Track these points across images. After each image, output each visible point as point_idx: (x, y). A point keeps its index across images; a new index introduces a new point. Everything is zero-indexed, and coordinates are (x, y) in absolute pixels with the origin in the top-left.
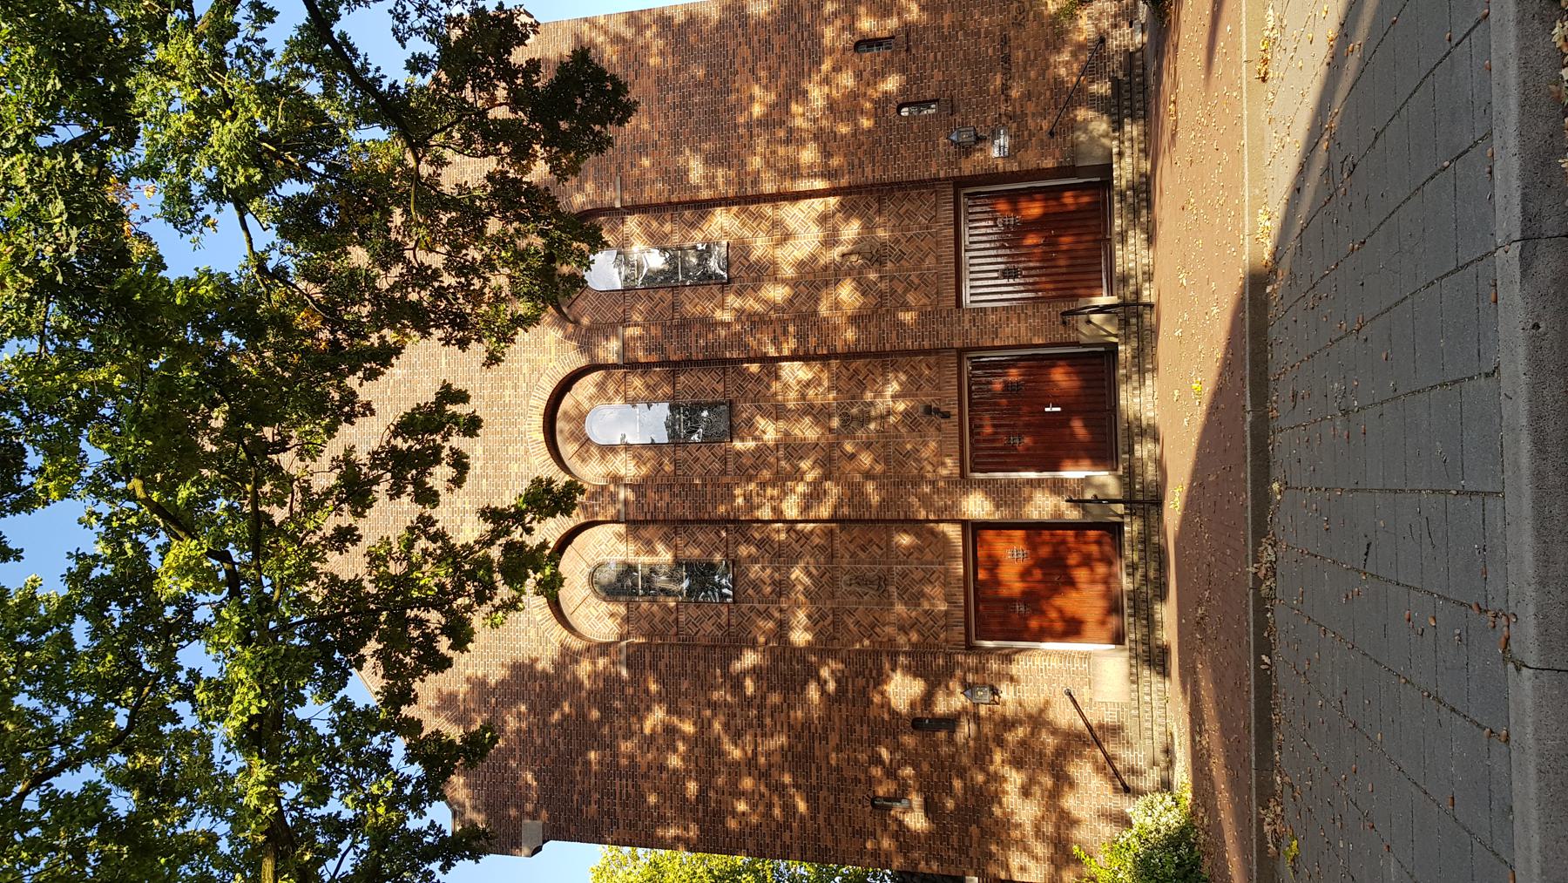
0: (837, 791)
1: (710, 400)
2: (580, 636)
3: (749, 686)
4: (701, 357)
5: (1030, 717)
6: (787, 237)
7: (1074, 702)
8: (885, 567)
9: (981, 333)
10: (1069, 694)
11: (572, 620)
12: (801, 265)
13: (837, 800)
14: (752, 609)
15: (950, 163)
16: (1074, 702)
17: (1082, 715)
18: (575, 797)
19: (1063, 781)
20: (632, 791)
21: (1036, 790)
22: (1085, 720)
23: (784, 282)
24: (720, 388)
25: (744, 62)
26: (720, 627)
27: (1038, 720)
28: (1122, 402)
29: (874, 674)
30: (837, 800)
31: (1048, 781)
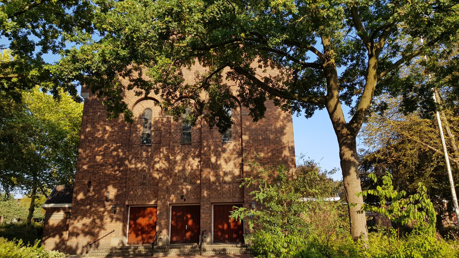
0: (93, 173)
1: (192, 138)
2: (133, 109)
3: (115, 153)
4: (202, 136)
5: (102, 225)
6: (226, 162)
7: (111, 232)
8: (148, 184)
9: (204, 209)
10: (114, 231)
11: (138, 105)
12: (220, 165)
13: (91, 173)
14: (139, 150)
15: (247, 201)
16: (111, 232)
17: (103, 237)
18: (94, 106)
19: (86, 234)
20: (95, 121)
21: (85, 227)
22: (101, 238)
23: (217, 161)
24: (195, 141)
25: (277, 147)
26: (135, 142)
27: (102, 227)
28: (173, 250)
29: (121, 182)
30: (91, 173)
31: (87, 230)
